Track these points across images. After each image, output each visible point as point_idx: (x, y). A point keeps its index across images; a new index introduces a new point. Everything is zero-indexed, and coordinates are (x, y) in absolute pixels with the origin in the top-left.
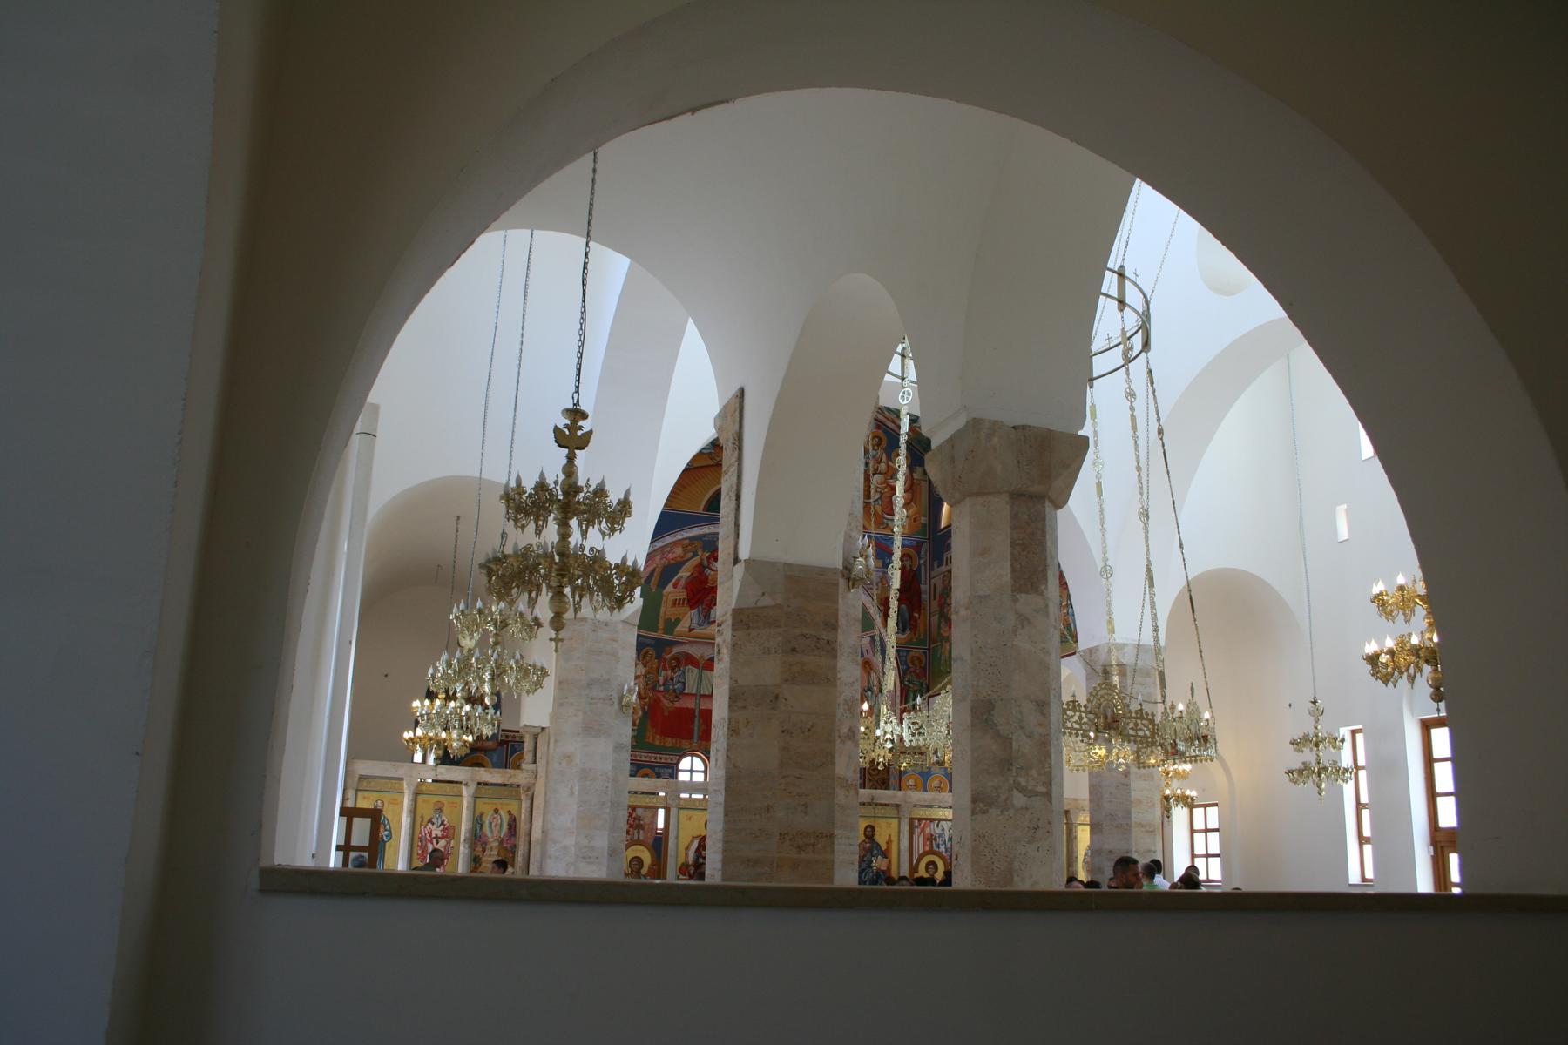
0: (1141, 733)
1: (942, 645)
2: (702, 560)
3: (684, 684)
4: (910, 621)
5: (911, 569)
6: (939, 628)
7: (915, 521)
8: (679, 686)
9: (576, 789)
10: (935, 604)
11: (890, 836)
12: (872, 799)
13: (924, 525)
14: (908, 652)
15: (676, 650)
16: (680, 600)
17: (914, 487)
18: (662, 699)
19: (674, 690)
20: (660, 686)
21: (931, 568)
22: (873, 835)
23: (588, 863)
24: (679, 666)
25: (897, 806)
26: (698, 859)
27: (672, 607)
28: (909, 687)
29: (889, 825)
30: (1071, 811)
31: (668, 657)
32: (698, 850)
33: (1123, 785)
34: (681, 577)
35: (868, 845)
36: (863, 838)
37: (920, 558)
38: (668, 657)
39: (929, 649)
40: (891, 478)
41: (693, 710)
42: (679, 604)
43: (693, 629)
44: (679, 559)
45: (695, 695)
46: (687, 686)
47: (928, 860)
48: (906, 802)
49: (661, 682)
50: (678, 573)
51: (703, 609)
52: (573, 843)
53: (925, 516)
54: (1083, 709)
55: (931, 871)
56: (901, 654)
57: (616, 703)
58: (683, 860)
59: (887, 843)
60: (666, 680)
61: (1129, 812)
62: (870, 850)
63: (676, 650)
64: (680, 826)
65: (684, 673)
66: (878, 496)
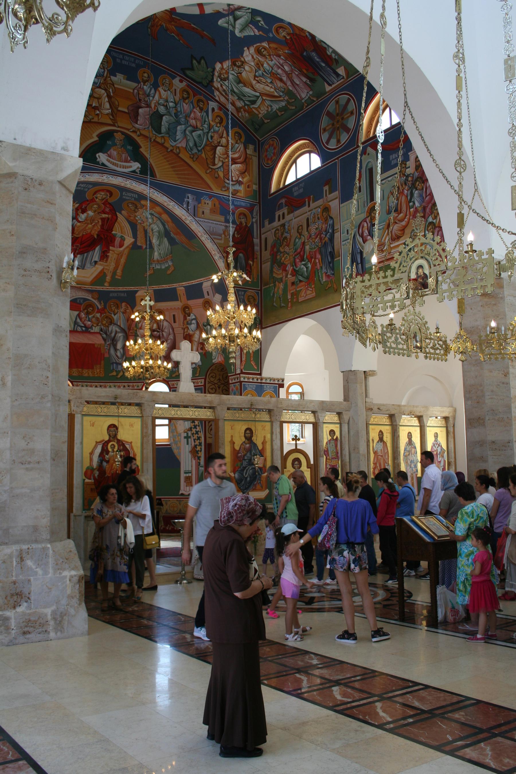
0: (438, 352)
1: (275, 286)
4: (246, 267)
5: (246, 225)
6: (272, 271)
7: (248, 187)
9: (9, 379)
10: (266, 255)
11: (265, 437)
12: (252, 405)
13: (255, 191)
14: (245, 292)
17: (247, 160)
21: (262, 225)
22: (252, 436)
23: (27, 469)
25: (270, 411)
26: (101, 463)
29: (264, 428)
30: (396, 415)
32: (101, 455)
33: (503, 383)
35: (248, 445)
36: (243, 439)
37: (253, 218)
39: (261, 290)
47: (291, 461)
48: (277, 408)
52: (8, 445)
53: (256, 184)
54: (398, 331)
55: (296, 466)
56: (240, 293)
57: (54, 276)
58: (88, 465)
59: (263, 443)
61: (509, 407)
62: (249, 450)
64: (85, 432)
66: (220, 164)
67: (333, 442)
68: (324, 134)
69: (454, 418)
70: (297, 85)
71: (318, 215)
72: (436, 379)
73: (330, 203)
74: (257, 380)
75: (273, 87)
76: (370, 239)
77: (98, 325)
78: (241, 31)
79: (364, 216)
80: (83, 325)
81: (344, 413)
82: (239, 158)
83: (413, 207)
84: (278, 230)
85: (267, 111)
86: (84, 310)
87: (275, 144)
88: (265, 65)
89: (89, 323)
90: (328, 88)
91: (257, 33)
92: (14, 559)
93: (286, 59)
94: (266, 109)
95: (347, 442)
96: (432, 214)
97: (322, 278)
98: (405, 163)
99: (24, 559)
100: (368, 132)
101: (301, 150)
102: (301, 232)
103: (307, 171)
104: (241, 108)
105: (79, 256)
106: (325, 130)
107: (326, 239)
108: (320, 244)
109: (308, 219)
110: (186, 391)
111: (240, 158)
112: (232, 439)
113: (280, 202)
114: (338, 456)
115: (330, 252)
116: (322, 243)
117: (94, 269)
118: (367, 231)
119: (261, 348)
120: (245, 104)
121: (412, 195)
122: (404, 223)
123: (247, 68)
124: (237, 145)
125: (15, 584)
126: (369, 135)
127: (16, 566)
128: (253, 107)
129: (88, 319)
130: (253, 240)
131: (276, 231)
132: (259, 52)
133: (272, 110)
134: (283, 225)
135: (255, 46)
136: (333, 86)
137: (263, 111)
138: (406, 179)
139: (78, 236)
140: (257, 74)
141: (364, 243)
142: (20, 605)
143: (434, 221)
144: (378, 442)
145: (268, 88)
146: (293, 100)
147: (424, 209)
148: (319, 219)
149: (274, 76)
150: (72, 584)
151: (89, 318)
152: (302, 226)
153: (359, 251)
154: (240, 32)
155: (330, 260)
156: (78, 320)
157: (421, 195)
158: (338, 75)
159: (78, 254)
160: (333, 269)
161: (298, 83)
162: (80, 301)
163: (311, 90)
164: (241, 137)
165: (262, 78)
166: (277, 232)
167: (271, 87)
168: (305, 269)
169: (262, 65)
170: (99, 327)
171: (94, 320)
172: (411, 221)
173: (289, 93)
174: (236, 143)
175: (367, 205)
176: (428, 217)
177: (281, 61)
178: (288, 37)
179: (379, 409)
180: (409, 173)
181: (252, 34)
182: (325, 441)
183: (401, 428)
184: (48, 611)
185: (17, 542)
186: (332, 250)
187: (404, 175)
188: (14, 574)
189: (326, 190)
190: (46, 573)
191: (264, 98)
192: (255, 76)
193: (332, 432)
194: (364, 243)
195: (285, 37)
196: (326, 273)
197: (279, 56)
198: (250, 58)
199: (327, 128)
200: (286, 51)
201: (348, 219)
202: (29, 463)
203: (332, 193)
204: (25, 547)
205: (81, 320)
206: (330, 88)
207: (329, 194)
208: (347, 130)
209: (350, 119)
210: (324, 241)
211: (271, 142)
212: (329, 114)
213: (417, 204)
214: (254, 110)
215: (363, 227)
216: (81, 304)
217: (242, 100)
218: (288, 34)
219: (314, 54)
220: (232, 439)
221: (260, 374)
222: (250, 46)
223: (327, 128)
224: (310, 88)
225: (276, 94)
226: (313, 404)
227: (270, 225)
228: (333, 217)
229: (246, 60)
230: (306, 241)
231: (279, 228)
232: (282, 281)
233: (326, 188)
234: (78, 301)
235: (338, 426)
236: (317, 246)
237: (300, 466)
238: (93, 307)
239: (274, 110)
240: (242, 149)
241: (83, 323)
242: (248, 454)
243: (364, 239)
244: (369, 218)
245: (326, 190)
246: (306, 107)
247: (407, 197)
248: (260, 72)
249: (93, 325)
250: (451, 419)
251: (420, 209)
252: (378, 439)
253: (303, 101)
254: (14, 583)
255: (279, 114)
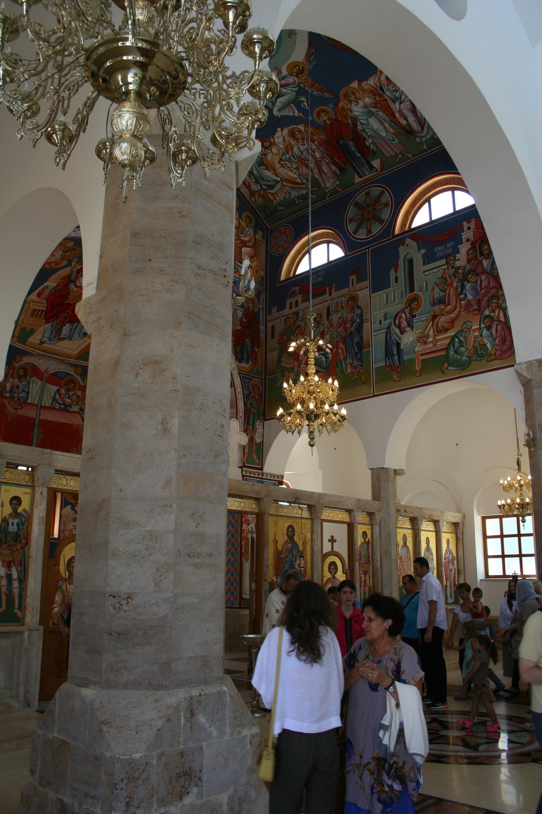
2: (72, 272)
3: (28, 393)
5: (253, 310)
8: (23, 395)
9: (175, 423)
11: (305, 537)
14: (250, 379)
15: (26, 360)
16: (39, 310)
18: (7, 405)
19: (19, 399)
20: (6, 392)
21: (269, 312)
22: (294, 535)
23: (196, 566)
24: (25, 375)
27: (30, 317)
28: (250, 409)
30: (419, 518)
31: (17, 365)
34: (47, 287)
35: (290, 545)
36: (286, 538)
37: (259, 304)
38: (17, 365)
39: (265, 379)
40: (241, 234)
41: (34, 420)
42: (37, 315)
43: (44, 343)
44: (53, 265)
45: (36, 405)
46: (30, 395)
47: (329, 562)
49: (8, 388)
50: (46, 280)
51: (57, 324)
53: (263, 271)
60: (12, 388)
62: (291, 551)
63: (26, 360)
65: (29, 383)
67: (365, 544)
68: (351, 224)
69: (463, 525)
70: (325, 173)
71: (341, 304)
72: (439, 483)
73: (358, 293)
74: (259, 475)
75: (297, 173)
76: (409, 330)
77: (78, 404)
78: (280, 110)
79: (401, 306)
80: (62, 402)
81: (376, 513)
82: (249, 241)
83: (464, 300)
84: (289, 318)
85: (284, 197)
86: (65, 385)
87: (288, 232)
88: (294, 149)
89: (69, 400)
90: (357, 180)
91: (296, 114)
92: (182, 714)
93: (320, 144)
94: (284, 195)
95: (378, 546)
96: (488, 307)
97: (346, 369)
98: (453, 255)
99: (195, 712)
100: (403, 224)
101: (318, 239)
102: (320, 321)
103: (325, 261)
104: (256, 192)
105: (68, 325)
106: (351, 220)
107: (352, 329)
108: (344, 334)
109: (328, 308)
110: (234, 478)
111: (250, 242)
112: (275, 538)
113: (293, 290)
114: (369, 561)
115: (358, 342)
116: (346, 332)
117: (82, 341)
118: (405, 322)
119: (263, 441)
120: (262, 189)
121: (463, 287)
122: (453, 315)
123: (274, 150)
124: (247, 228)
125: (182, 757)
126: (405, 228)
127: (184, 725)
128: (270, 193)
129: (67, 396)
130: (259, 328)
131: (286, 318)
132: (292, 135)
133: (290, 197)
134: (297, 313)
135: (290, 127)
136: (364, 178)
137: (280, 197)
138: (455, 271)
139: (71, 302)
140: (283, 158)
141: (402, 334)
142: (188, 793)
143: (492, 314)
144: (402, 547)
145: (291, 174)
146: (316, 189)
147: (479, 302)
148: (342, 308)
149: (303, 162)
150: (253, 749)
151: (69, 395)
152: (320, 314)
153: (395, 342)
154: (278, 111)
155: (356, 350)
156: (57, 396)
157: (474, 288)
158: (371, 167)
159: (67, 323)
160: (361, 360)
161: (326, 171)
162: (61, 375)
163: (339, 180)
164: (252, 222)
165: (287, 163)
166: (288, 320)
167: (295, 173)
168: (324, 359)
169: (292, 149)
170: (79, 406)
171: (74, 397)
172: (461, 313)
173: (315, 182)
174: (247, 226)
175: (406, 296)
176: (485, 310)
177: (314, 147)
178: (328, 123)
179: (405, 511)
180: (459, 266)
181: (291, 114)
182: (359, 543)
183: (422, 533)
184: (224, 798)
185: (181, 684)
186: (360, 341)
187: (454, 267)
188: (181, 740)
189: (353, 280)
190: (222, 734)
191: (284, 184)
192: (281, 160)
193: (364, 534)
194: (402, 334)
195: (325, 121)
196: (352, 364)
197: (313, 141)
198: (281, 140)
199: (355, 219)
200: (322, 137)
201: (380, 310)
202: (199, 555)
203: (359, 283)
204: (195, 692)
205: (60, 396)
206: (360, 179)
207: (357, 283)
208: (381, 221)
209: (384, 210)
210: (350, 331)
211: (283, 230)
212: (357, 205)
213: (469, 297)
214: (269, 195)
215: (400, 317)
216: (62, 379)
217: (260, 183)
218: (329, 119)
219: (351, 143)
220: (275, 538)
221: (261, 469)
222: (285, 127)
223: (355, 219)
224: (338, 177)
225: (299, 181)
226: (351, 502)
227: (278, 313)
228: (362, 306)
229: (276, 141)
230: (326, 330)
231: (291, 316)
232: (293, 371)
233: (354, 277)
234: (59, 376)
235: (370, 527)
236: (341, 336)
237: (336, 571)
238: (74, 384)
239: (292, 198)
240: (252, 233)
241: (62, 401)
242: (290, 556)
243: (402, 330)
244: (409, 309)
245: (353, 280)
246: (329, 197)
247: (456, 289)
248: (288, 156)
249: (72, 404)
250: (461, 525)
251: (473, 302)
252: (402, 543)
253: (327, 191)
254: (182, 754)
255: (297, 202)
